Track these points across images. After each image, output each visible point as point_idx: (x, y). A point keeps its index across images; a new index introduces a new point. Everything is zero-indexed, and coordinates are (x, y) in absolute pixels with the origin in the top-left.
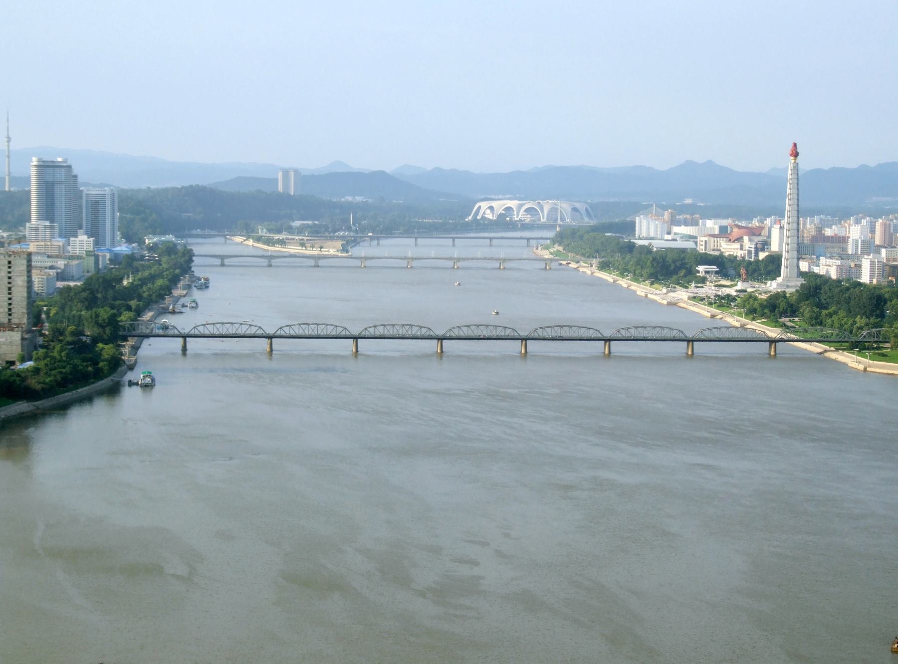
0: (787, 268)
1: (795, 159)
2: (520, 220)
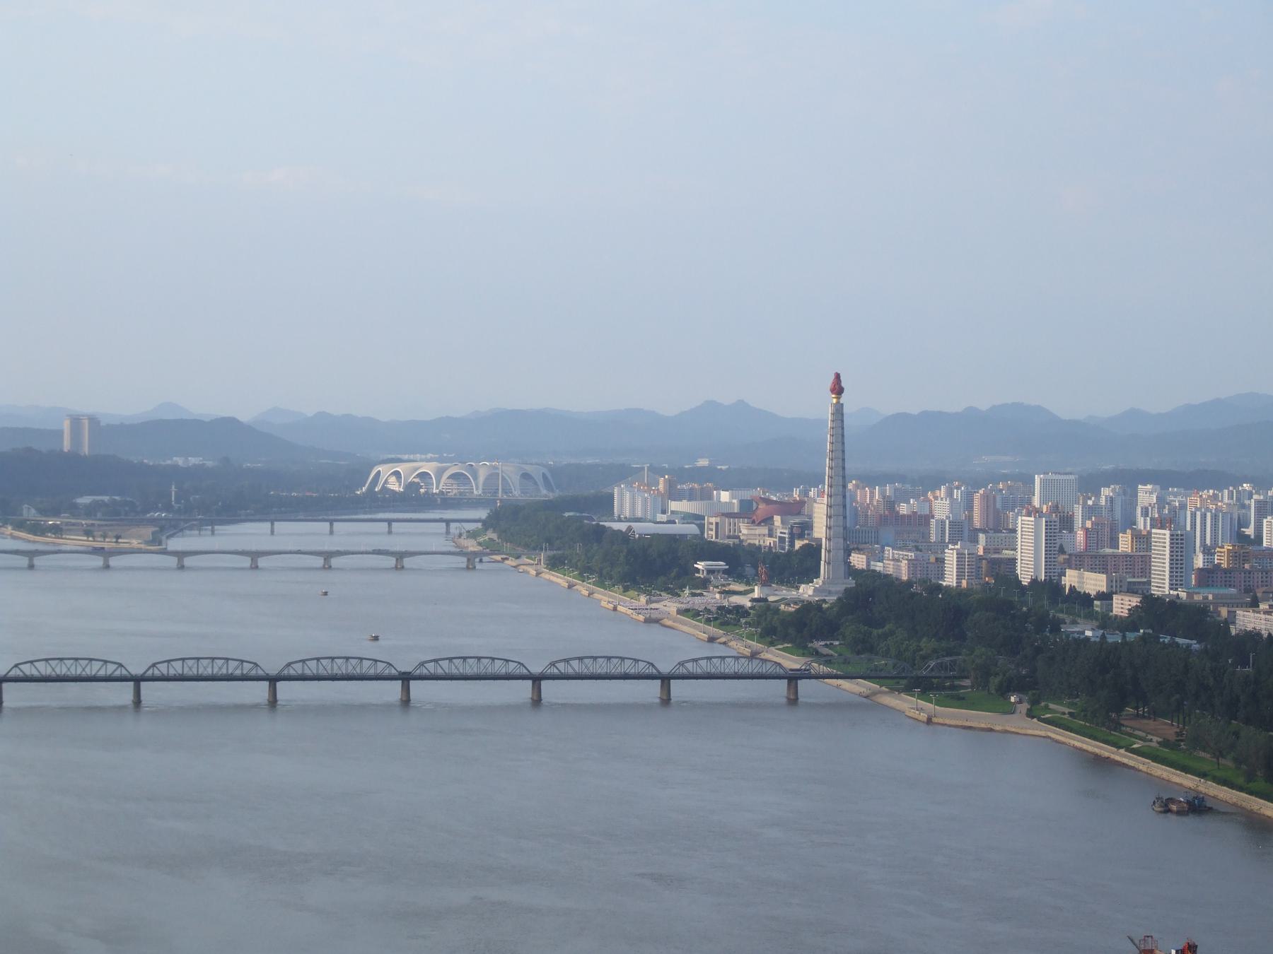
0: (829, 563)
1: (838, 398)
2: (441, 492)
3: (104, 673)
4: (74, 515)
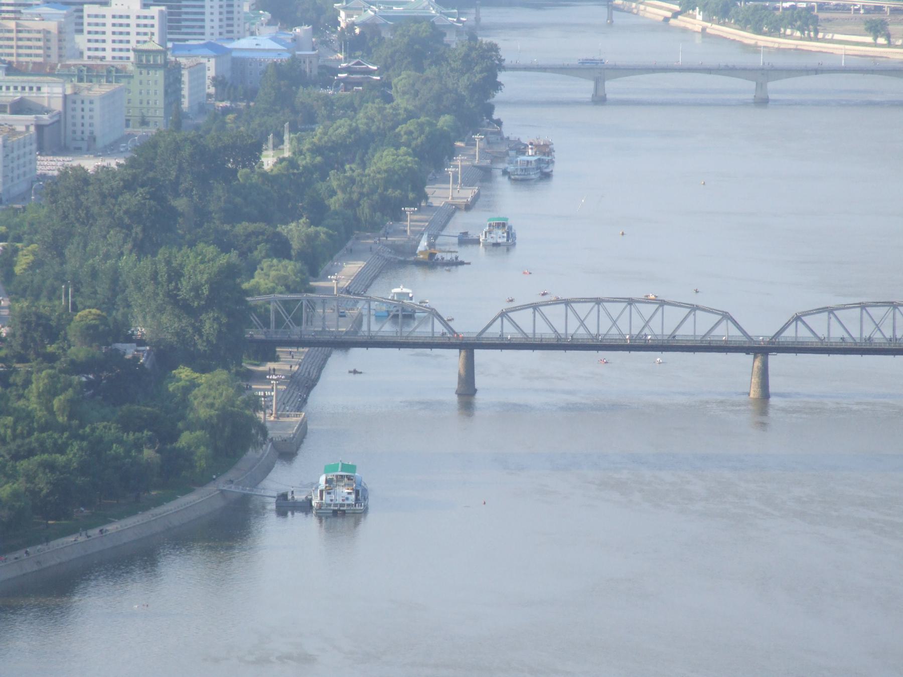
3: (793, 335)
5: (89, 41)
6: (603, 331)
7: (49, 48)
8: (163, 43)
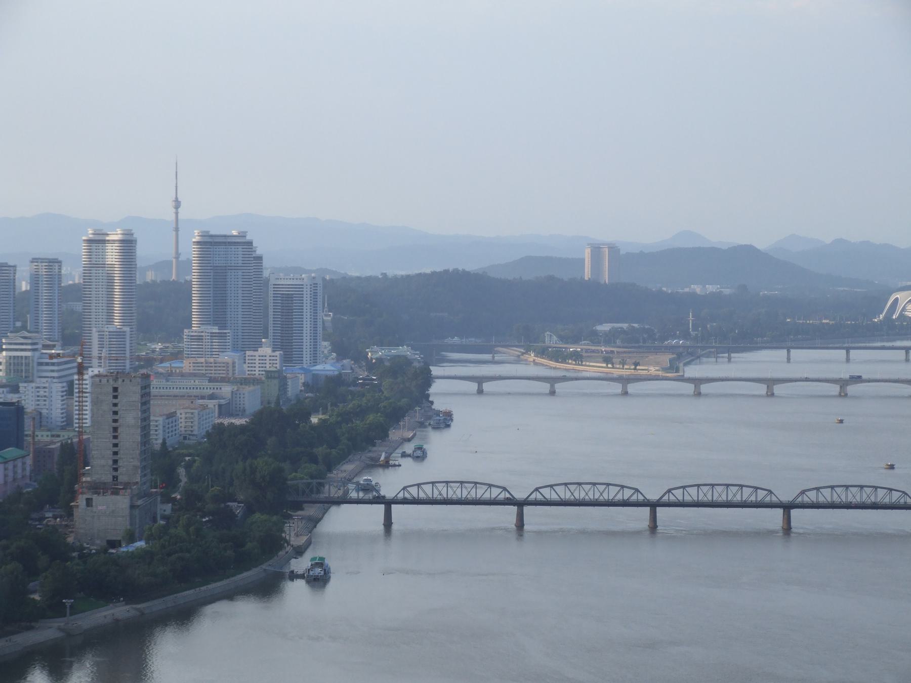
4: (594, 343)
5: (249, 367)
6: (567, 497)
7: (228, 371)
8: (281, 366)
